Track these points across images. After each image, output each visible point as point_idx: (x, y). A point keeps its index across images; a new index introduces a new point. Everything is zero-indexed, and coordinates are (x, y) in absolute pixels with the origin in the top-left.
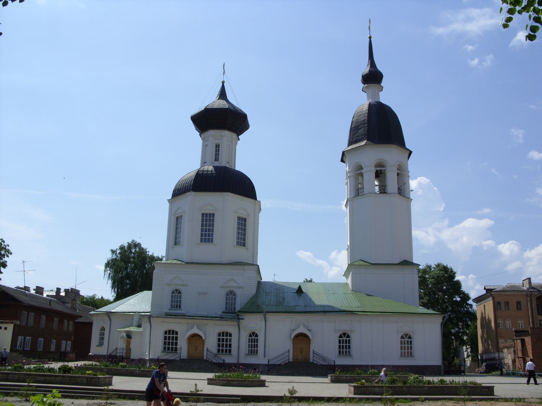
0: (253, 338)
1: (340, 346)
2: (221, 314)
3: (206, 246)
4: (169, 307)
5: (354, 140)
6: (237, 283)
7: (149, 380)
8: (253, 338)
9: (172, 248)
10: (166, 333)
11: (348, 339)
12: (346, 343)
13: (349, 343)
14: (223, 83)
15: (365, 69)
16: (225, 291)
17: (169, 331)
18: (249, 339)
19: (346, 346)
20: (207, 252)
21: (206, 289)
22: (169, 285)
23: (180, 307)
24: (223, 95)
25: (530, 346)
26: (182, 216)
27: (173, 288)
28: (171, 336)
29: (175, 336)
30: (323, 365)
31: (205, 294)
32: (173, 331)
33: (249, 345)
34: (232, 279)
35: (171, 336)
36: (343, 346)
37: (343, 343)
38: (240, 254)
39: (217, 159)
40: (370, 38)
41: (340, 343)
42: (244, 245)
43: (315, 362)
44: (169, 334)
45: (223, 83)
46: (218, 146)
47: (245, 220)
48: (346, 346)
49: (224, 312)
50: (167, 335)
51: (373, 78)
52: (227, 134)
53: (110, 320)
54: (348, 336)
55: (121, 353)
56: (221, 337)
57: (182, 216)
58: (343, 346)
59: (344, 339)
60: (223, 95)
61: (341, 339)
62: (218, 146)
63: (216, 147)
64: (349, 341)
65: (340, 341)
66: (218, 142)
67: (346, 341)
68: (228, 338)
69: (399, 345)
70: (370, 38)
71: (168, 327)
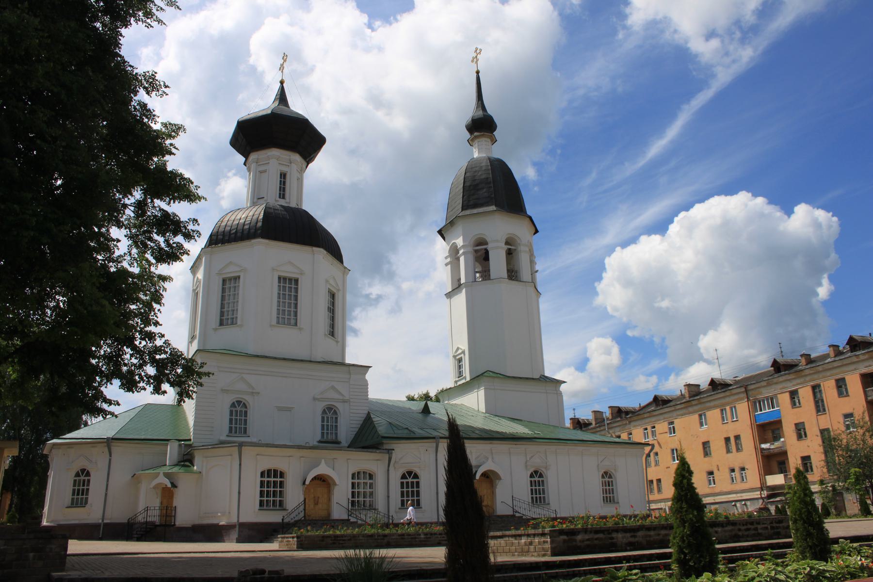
0: (82, 478)
1: (402, 493)
3: (287, 332)
4: (227, 431)
5: (471, 203)
6: (340, 393)
7: (68, 552)
9: (215, 330)
11: (415, 480)
13: (418, 486)
14: (282, 82)
15: (469, 111)
16: (320, 406)
17: (269, 471)
18: (75, 481)
20: (286, 341)
21: (286, 402)
22: (224, 391)
23: (245, 432)
24: (282, 97)
26: (237, 278)
27: (232, 398)
31: (289, 409)
32: (275, 471)
34: (333, 388)
36: (408, 492)
38: (324, 349)
39: (282, 196)
40: (478, 72)
41: (402, 487)
43: (517, 515)
44: (269, 476)
45: (282, 82)
46: (283, 176)
47: (297, 281)
49: (320, 442)
50: (266, 479)
52: (297, 157)
53: (110, 456)
54: (416, 476)
55: (155, 517)
56: (266, 479)
57: (237, 278)
58: (408, 492)
59: (410, 480)
60: (282, 97)
61: (405, 481)
62: (283, 176)
63: (284, 195)
64: (418, 483)
65: (402, 483)
66: (284, 169)
70: (478, 72)
71: (353, 469)
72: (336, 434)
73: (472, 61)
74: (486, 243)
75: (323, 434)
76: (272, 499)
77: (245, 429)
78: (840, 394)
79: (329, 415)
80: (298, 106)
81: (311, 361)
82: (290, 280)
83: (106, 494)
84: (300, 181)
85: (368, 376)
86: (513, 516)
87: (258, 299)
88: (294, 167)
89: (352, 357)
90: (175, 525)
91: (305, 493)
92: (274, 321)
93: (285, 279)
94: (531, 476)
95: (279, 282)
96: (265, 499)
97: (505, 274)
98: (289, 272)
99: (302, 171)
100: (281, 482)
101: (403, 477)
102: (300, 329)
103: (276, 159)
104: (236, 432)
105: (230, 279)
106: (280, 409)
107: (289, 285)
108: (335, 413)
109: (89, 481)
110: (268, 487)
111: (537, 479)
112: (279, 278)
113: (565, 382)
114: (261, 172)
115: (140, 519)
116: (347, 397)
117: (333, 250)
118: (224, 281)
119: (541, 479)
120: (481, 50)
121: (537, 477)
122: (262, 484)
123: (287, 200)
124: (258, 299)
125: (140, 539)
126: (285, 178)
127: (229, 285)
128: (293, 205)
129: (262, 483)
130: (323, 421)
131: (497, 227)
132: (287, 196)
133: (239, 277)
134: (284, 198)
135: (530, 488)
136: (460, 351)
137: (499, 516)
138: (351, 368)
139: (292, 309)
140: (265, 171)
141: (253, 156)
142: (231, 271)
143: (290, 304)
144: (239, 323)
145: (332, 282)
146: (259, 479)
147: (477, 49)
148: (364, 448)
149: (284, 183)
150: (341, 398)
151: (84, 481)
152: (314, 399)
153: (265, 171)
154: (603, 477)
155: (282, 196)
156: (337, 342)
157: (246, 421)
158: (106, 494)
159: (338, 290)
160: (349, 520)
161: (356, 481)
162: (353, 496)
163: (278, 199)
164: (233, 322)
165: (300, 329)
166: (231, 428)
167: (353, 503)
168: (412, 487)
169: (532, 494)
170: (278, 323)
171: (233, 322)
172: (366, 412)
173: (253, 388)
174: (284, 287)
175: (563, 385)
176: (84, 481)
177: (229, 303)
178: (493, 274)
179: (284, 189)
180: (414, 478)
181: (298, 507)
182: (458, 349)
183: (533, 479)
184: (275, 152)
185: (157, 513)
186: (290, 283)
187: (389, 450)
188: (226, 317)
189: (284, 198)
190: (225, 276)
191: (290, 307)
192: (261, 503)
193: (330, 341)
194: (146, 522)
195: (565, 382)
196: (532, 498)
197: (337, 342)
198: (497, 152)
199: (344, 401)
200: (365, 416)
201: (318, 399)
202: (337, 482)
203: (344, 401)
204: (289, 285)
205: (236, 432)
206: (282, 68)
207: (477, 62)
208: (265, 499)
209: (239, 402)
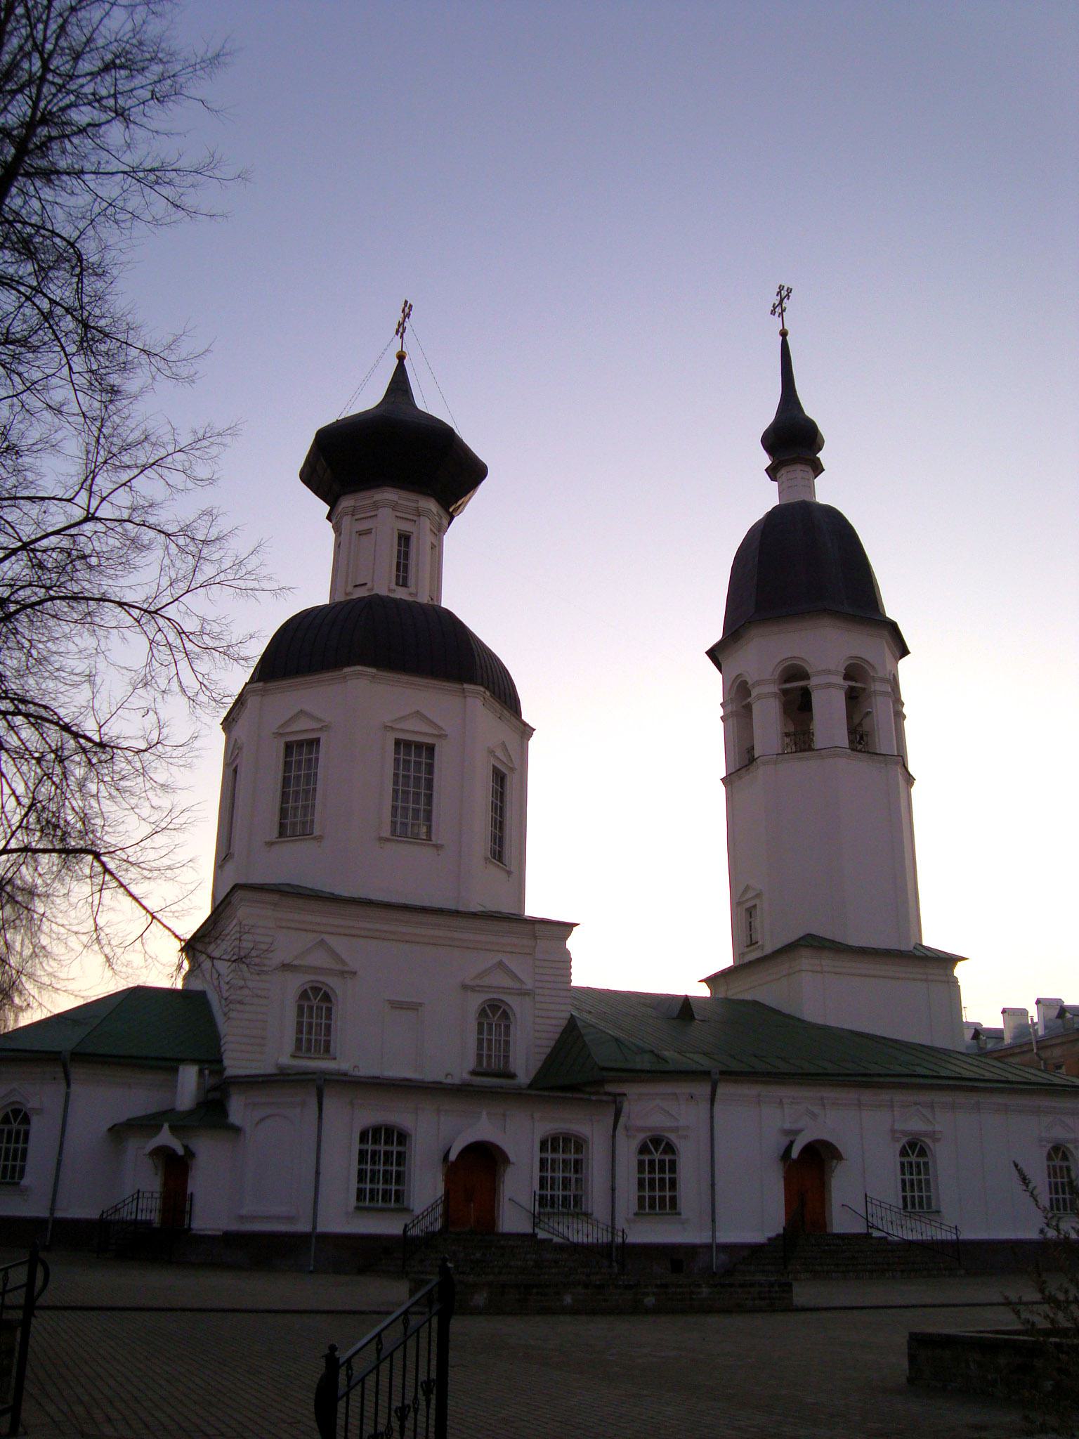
2: (466, 1076)
4: (289, 1047)
6: (514, 977)
8: (15, 1126)
10: (363, 1137)
11: (667, 1158)
12: (662, 1170)
14: (401, 357)
16: (476, 1002)
18: (902, 1164)
19: (652, 1188)
20: (404, 873)
23: (327, 1050)
24: (400, 384)
25: (339, 1415)
28: (382, 1148)
29: (395, 1148)
30: (910, 1243)
31: (413, 1007)
33: (928, 1190)
34: (501, 964)
35: (382, 1148)
37: (652, 1170)
38: (482, 893)
39: (403, 581)
42: (500, 859)
43: (876, 1234)
44: (375, 1141)
45: (401, 357)
47: (431, 749)
48: (652, 1188)
50: (370, 1147)
51: (793, 442)
52: (432, 505)
54: (670, 1148)
56: (549, 1156)
60: (400, 384)
61: (646, 1158)
62: (404, 539)
63: (405, 578)
66: (406, 527)
67: (662, 1162)
68: (395, 1148)
69: (354, 1184)
72: (506, 1057)
73: (773, 313)
74: (806, 676)
75: (480, 1056)
76: (381, 1186)
77: (328, 1043)
79: (494, 1020)
80: (429, 399)
81: (457, 913)
82: (419, 746)
83: (59, 1163)
84: (437, 549)
85: (572, 943)
86: (868, 1235)
87: (356, 782)
88: (426, 523)
89: (535, 907)
90: (190, 1229)
91: (448, 1181)
92: (386, 833)
93: (408, 744)
94: (903, 1153)
95: (397, 751)
96: (368, 1186)
97: (842, 739)
98: (416, 730)
99: (440, 530)
100: (399, 1174)
101: (643, 1149)
102: (438, 847)
103: (389, 507)
104: (309, 1050)
105: (300, 744)
106: (397, 1005)
107: (415, 758)
108: (505, 1015)
109: (27, 1133)
110: (374, 1163)
111: (913, 1158)
112: (398, 743)
113: (963, 959)
114: (361, 533)
115: (125, 1214)
116: (529, 984)
118: (289, 747)
119: (921, 1160)
120: (789, 291)
121: (915, 1152)
122: (362, 1154)
123: (412, 590)
124: (356, 782)
126: (407, 545)
127: (300, 754)
128: (424, 599)
129: (362, 1153)
130: (480, 1032)
131: (824, 647)
132: (412, 580)
133: (318, 740)
134: (405, 585)
135: (899, 1177)
136: (750, 894)
137: (838, 1236)
138: (537, 926)
139: (485, 1052)
140: (369, 532)
141: (346, 503)
143: (417, 779)
144: (317, 832)
145: (499, 753)
146: (356, 1146)
147: (781, 288)
148: (564, 1088)
149: (407, 554)
150: (518, 985)
151: (18, 1133)
152: (465, 987)
153: (369, 532)
154: (1049, 1158)
155: (403, 581)
156: (509, 873)
157: (328, 1027)
158: (59, 1163)
159: (512, 769)
160: (534, 1235)
161: (549, 1156)
162: (542, 1186)
163: (393, 586)
164: (306, 832)
165: (438, 847)
166: (299, 1041)
167: (542, 1201)
168: (662, 1170)
169: (904, 1190)
170: (393, 833)
171: (306, 832)
172: (568, 1015)
173: (343, 962)
174: (407, 762)
175: (960, 964)
176: (18, 1133)
177: (294, 824)
178: (819, 741)
179: (406, 566)
180: (665, 1152)
181: (433, 1208)
182: (747, 888)
183: (906, 1160)
184: (389, 495)
185: (156, 1204)
187: (615, 1095)
188: (294, 818)
189: (405, 585)
191: (416, 801)
192: (360, 1194)
194: (135, 1222)
195: (963, 959)
196: (904, 1198)
197: (509, 873)
199: (523, 993)
200: (565, 1022)
201: (473, 989)
202: (512, 1158)
203: (523, 993)
204: (415, 758)
205: (309, 1050)
206: (401, 330)
207: (781, 314)
208: (368, 1186)
209: (316, 990)
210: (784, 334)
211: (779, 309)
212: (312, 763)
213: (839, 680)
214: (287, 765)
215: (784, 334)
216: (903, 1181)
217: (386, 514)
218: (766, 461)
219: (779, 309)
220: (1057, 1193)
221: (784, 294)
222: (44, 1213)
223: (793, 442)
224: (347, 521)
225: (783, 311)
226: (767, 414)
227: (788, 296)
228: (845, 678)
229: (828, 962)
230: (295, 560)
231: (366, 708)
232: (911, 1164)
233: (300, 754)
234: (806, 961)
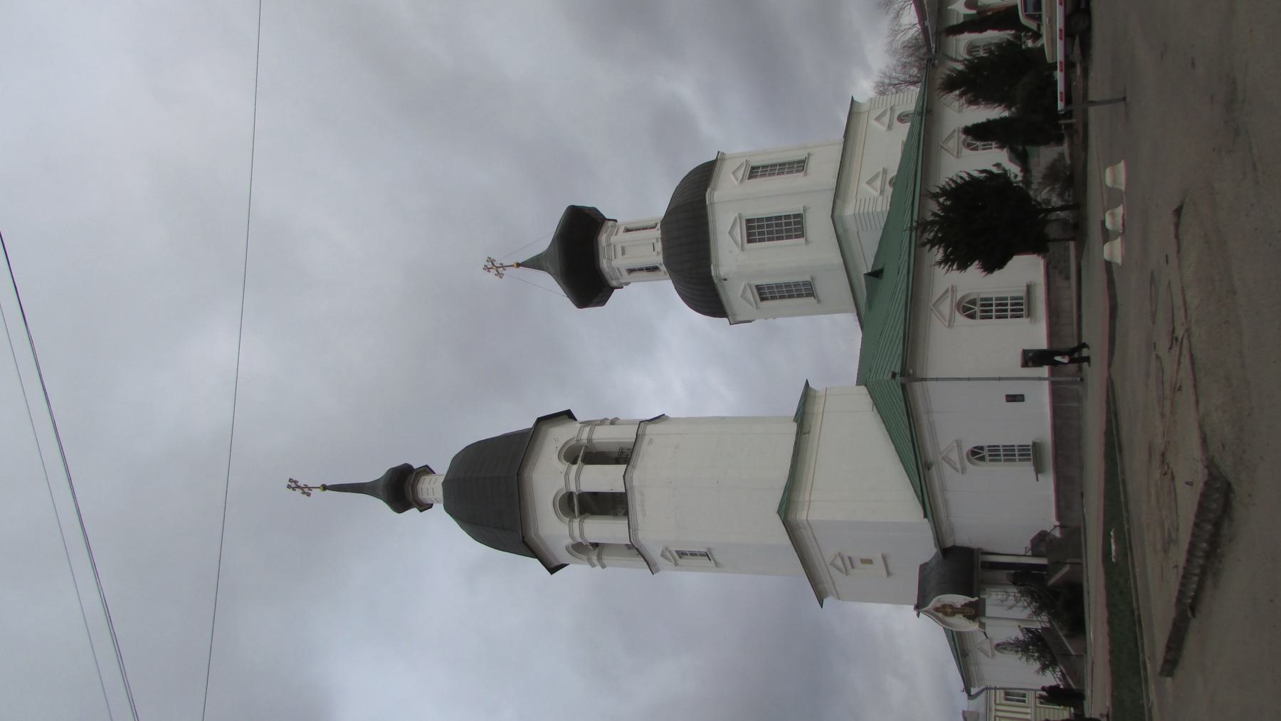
14: (519, 265)
18: (983, 318)
20: (819, 225)
24: (535, 263)
26: (759, 288)
39: (654, 269)
45: (519, 265)
51: (400, 489)
60: (535, 263)
73: (309, 495)
78: (1007, 396)
82: (748, 228)
87: (779, 260)
92: (802, 240)
93: (749, 235)
95: (754, 241)
102: (805, 209)
105: (760, 294)
107: (759, 230)
112: (749, 241)
117: (703, 177)
118: (763, 299)
120: (291, 480)
124: (779, 260)
125: (1111, 606)
127: (764, 293)
131: (549, 477)
133: (757, 286)
140: (623, 249)
141: (614, 283)
142: (752, 295)
143: (777, 225)
144: (808, 278)
147: (289, 487)
151: (983, 305)
170: (802, 236)
183: (979, 314)
184: (604, 264)
186: (753, 228)
190: (758, 298)
193: (812, 165)
198: (442, 467)
204: (759, 230)
207: (310, 488)
210: (325, 488)
211: (306, 490)
212: (770, 287)
213: (575, 467)
214: (773, 298)
215: (325, 488)
216: (998, 317)
217: (615, 263)
218: (414, 512)
219: (306, 490)
220: (998, 305)
221: (294, 485)
222: (1046, 384)
223: (400, 489)
224: (622, 281)
225: (306, 486)
226: (379, 507)
227: (296, 482)
228: (574, 462)
229: (804, 497)
230: (648, 300)
231: (732, 258)
232: (983, 311)
233: (764, 293)
234: (802, 515)
